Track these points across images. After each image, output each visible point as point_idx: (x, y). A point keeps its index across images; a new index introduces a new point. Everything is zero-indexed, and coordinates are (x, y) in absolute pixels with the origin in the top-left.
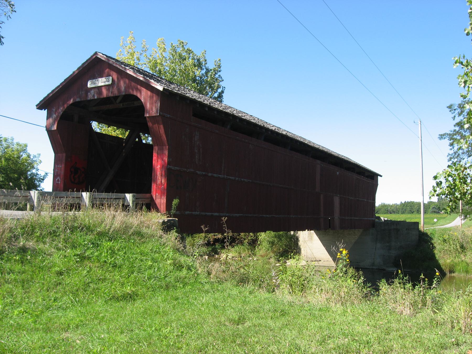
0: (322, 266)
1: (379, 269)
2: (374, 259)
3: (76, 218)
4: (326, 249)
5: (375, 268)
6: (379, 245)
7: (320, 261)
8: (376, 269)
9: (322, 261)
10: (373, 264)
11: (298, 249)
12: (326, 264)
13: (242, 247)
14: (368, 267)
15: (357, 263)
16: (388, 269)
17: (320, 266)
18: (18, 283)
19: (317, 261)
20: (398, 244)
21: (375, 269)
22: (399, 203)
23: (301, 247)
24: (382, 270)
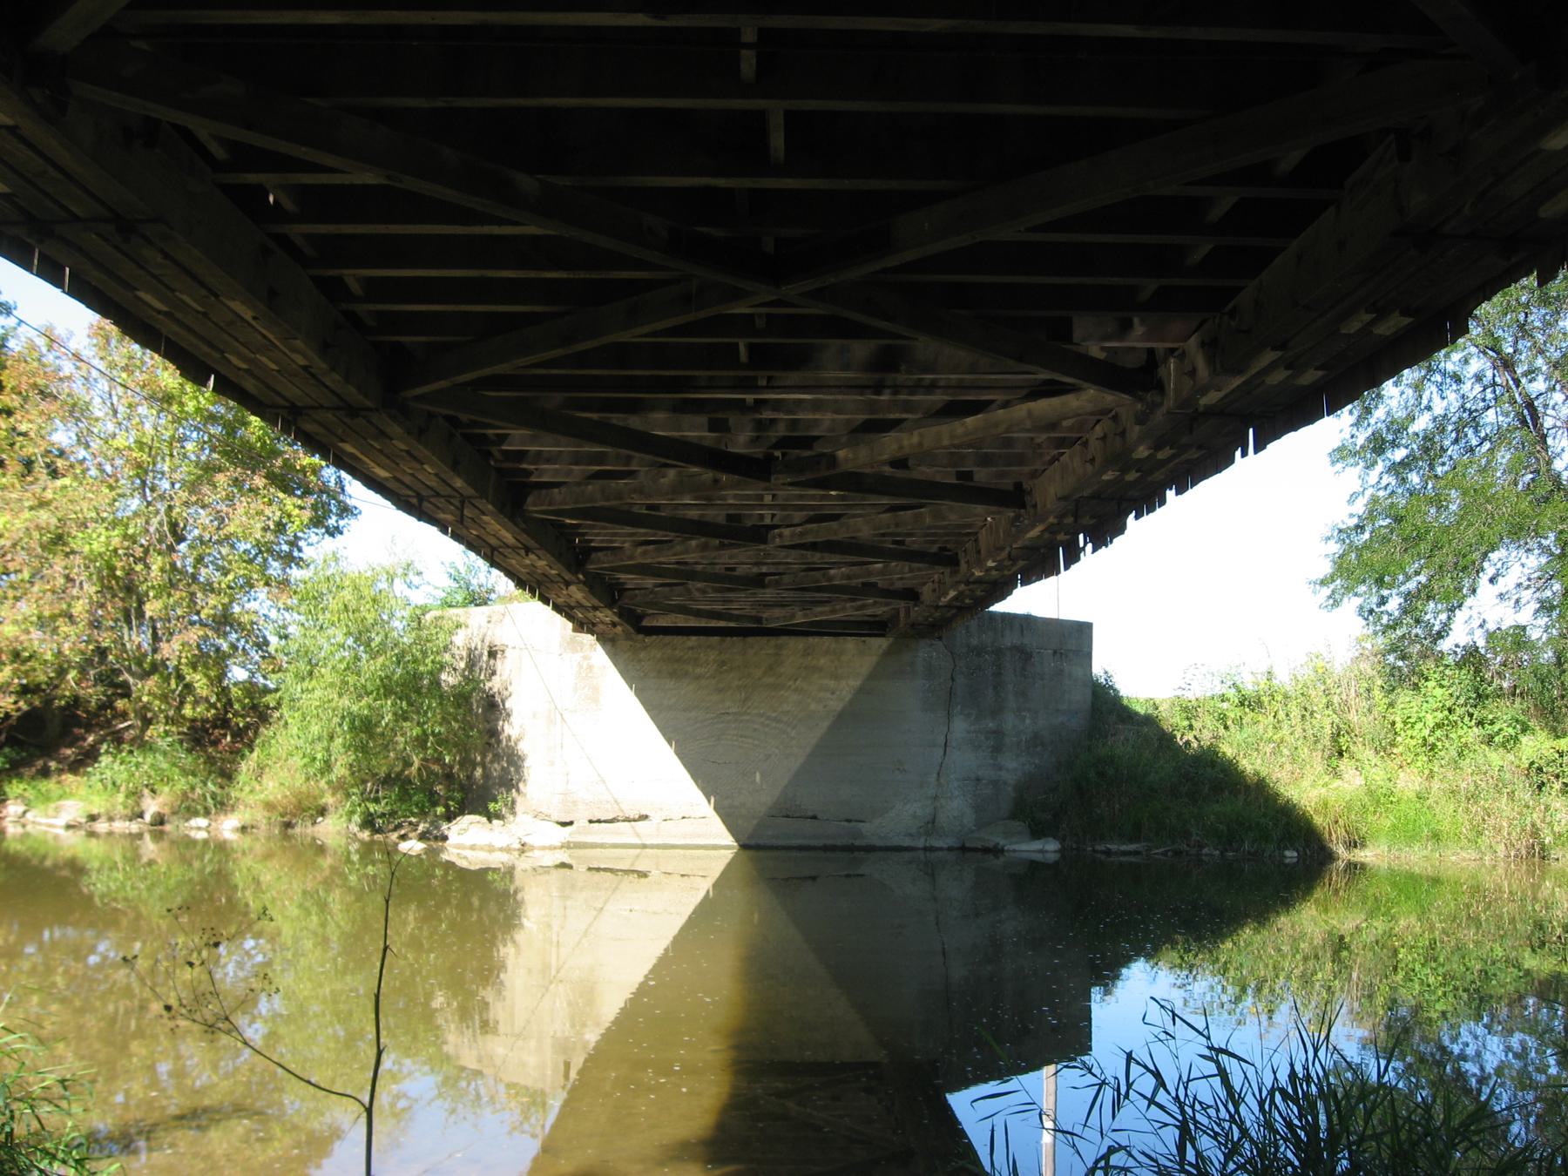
0: (653, 847)
1: (963, 849)
2: (936, 798)
3: (259, 1140)
4: (678, 753)
5: (945, 846)
6: (960, 726)
7: (644, 817)
8: (950, 849)
9: (656, 817)
10: (931, 825)
11: (497, 758)
12: (676, 833)
13: (149, 760)
14: (907, 842)
15: (849, 821)
16: (1016, 847)
17: (644, 846)
18: (433, 732)
19: (628, 820)
20: (1028, 721)
21: (941, 849)
22: (1116, 540)
23: (523, 748)
24: (986, 850)
